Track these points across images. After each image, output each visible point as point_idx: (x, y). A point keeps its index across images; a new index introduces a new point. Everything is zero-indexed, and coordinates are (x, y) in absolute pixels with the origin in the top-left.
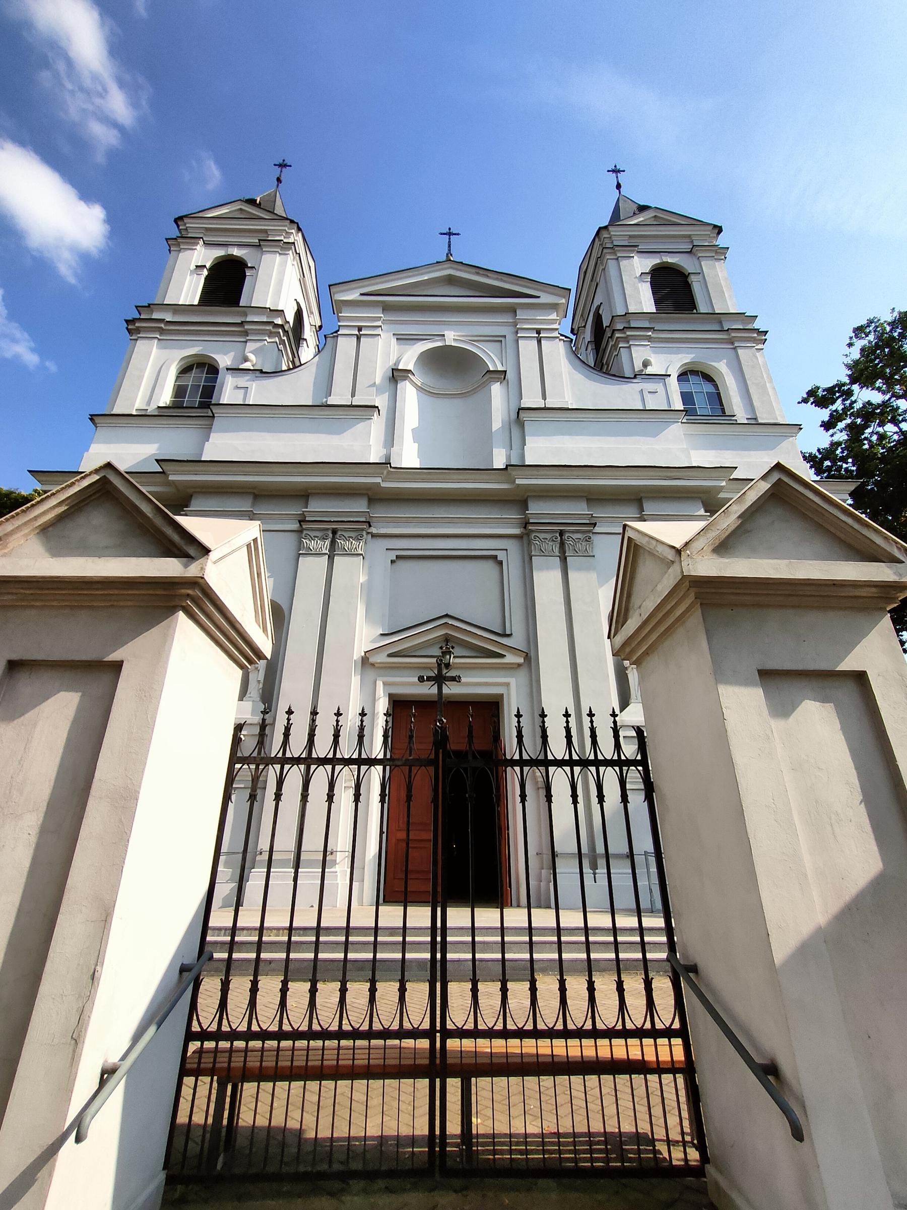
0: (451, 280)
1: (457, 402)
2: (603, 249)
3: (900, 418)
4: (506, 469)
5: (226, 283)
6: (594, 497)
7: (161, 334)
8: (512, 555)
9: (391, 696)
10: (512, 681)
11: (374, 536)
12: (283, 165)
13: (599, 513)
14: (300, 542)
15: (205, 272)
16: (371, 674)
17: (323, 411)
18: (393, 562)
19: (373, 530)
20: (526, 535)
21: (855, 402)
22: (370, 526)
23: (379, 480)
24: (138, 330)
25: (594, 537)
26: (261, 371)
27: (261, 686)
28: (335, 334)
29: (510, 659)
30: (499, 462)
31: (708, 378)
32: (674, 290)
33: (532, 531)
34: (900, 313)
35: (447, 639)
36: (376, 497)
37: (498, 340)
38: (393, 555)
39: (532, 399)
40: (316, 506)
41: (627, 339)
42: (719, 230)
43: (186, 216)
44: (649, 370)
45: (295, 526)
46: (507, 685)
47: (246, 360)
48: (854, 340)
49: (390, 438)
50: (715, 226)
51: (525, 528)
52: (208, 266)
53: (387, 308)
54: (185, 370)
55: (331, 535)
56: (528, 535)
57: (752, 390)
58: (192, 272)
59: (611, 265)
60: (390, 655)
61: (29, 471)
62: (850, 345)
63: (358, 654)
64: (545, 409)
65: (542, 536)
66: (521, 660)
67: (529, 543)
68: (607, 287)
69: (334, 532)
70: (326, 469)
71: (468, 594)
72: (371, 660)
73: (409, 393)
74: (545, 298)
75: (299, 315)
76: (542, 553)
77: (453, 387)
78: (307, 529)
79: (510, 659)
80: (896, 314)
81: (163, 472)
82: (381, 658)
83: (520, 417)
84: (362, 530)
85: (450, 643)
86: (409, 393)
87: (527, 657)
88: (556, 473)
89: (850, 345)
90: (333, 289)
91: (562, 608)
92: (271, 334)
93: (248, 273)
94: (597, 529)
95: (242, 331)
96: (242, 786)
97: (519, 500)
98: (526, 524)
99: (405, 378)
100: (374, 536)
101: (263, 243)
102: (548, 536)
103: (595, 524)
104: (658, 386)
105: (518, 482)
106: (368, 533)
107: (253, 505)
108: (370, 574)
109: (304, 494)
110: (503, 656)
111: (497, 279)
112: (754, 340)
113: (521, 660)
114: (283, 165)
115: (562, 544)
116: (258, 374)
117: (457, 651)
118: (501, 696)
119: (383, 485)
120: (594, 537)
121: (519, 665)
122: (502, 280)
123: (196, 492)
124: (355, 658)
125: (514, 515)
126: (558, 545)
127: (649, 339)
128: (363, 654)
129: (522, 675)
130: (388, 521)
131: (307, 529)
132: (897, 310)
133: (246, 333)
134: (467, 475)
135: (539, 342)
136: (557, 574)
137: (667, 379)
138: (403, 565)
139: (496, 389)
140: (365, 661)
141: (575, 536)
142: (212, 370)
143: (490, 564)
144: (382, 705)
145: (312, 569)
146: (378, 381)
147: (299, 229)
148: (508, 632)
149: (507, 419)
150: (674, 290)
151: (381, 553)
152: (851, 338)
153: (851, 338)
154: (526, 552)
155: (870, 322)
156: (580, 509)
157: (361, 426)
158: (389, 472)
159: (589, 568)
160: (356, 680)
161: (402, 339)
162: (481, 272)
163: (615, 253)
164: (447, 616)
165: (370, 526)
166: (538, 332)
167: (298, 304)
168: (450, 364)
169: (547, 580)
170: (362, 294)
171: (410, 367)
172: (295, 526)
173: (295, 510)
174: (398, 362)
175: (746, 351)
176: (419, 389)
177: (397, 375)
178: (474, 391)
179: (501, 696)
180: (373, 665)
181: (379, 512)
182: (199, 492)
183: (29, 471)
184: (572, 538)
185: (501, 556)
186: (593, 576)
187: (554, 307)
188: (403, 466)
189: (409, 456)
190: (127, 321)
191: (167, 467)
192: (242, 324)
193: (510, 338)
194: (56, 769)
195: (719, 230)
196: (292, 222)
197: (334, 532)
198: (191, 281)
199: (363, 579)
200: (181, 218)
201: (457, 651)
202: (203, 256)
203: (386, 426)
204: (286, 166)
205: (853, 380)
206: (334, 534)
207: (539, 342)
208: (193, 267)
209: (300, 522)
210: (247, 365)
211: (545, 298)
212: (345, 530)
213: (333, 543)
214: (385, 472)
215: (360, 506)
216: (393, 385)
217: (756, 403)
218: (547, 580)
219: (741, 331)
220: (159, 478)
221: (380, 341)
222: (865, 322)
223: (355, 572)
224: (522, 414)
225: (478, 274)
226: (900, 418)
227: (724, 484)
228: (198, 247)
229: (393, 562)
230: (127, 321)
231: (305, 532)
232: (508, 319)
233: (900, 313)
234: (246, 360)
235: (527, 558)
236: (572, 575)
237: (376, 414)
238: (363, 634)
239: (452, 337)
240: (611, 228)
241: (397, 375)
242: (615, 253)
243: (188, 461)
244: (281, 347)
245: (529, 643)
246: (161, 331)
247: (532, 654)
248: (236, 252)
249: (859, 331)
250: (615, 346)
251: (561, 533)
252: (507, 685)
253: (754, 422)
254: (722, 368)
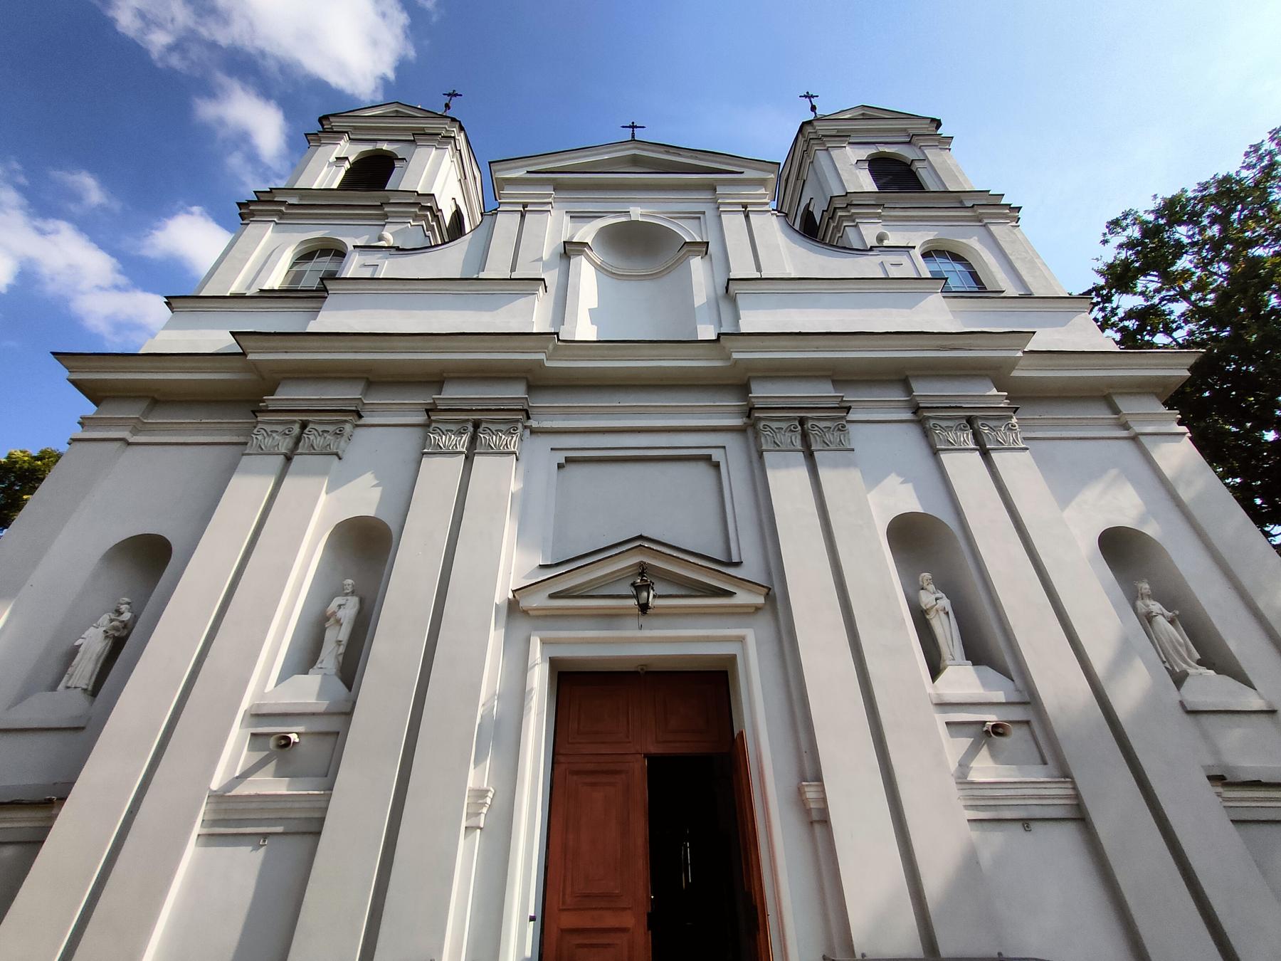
0: (635, 161)
1: (648, 285)
2: (811, 137)
3: (1174, 326)
4: (718, 340)
5: (372, 173)
6: (841, 375)
7: (280, 218)
8: (733, 455)
9: (554, 663)
10: (750, 634)
11: (534, 432)
12: (453, 95)
13: (849, 396)
14: (426, 438)
15: (347, 165)
16: (522, 626)
17: (471, 284)
18: (560, 466)
19: (533, 423)
20: (752, 424)
21: (1118, 307)
22: (529, 418)
23: (542, 356)
24: (252, 214)
25: (848, 426)
26: (398, 249)
27: (342, 649)
28: (495, 212)
29: (743, 598)
30: (707, 332)
31: (957, 258)
32: (896, 176)
33: (760, 419)
34: (1163, 199)
35: (642, 569)
36: (539, 381)
37: (697, 216)
38: (561, 457)
39: (742, 267)
40: (452, 393)
41: (851, 218)
42: (938, 123)
43: (334, 115)
44: (886, 243)
45: (421, 418)
46: (741, 640)
47: (381, 238)
48: (1109, 237)
49: (561, 307)
50: (933, 120)
51: (749, 417)
52: (351, 159)
53: (558, 187)
54: (306, 256)
55: (471, 429)
56: (754, 426)
57: (1018, 265)
58: (330, 164)
59: (821, 157)
60: (552, 596)
61: (53, 353)
62: (1105, 242)
63: (502, 594)
64: (761, 279)
65: (774, 425)
66: (760, 600)
67: (757, 435)
68: (818, 180)
69: (476, 425)
70: (473, 342)
71: (671, 508)
72: (524, 604)
73: (586, 274)
74: (749, 174)
75: (458, 215)
76: (777, 447)
77: (640, 268)
78: (435, 421)
79: (743, 598)
80: (1159, 201)
81: (244, 354)
82: (538, 601)
83: (730, 290)
84: (517, 421)
85: (649, 574)
86: (586, 274)
87: (769, 594)
88: (784, 343)
89: (1105, 242)
90: (494, 167)
91: (816, 521)
92: (416, 217)
93: (397, 164)
94: (851, 416)
95: (381, 214)
96: (280, 829)
97: (737, 384)
98: (749, 412)
99: (581, 253)
100: (534, 432)
101: (419, 137)
102: (784, 425)
103: (849, 409)
104: (903, 259)
105: (735, 356)
106: (525, 427)
107: (365, 393)
108: (527, 478)
109: (436, 378)
110: (729, 594)
111: (691, 157)
112: (1005, 216)
113: (760, 600)
114: (453, 95)
115: (805, 437)
116: (393, 252)
117: (660, 588)
118: (733, 659)
119: (548, 364)
120: (848, 426)
121: (757, 609)
122: (696, 158)
123: (285, 378)
124: (497, 600)
125: (732, 402)
126: (799, 437)
127: (879, 216)
128: (511, 595)
129: (764, 621)
130: (553, 412)
131: (435, 421)
132: (1160, 196)
133: (386, 216)
134: (666, 349)
135: (747, 217)
136: (803, 473)
137: (912, 251)
138: (575, 471)
139: (697, 264)
140: (513, 608)
141: (822, 424)
142: (339, 253)
143: (702, 468)
144: (539, 678)
145: (440, 474)
146: (545, 256)
147: (462, 129)
148: (735, 559)
149: (712, 294)
150: (896, 176)
151: (543, 453)
152: (1104, 234)
153: (1104, 234)
154: (752, 445)
155: (1125, 216)
156: (823, 391)
157: (521, 302)
158: (556, 348)
159: (849, 464)
160: (495, 636)
161: (575, 216)
162: (672, 150)
163: (823, 144)
164: (641, 537)
165: (529, 418)
166: (745, 206)
167: (457, 206)
168: (637, 246)
169: (788, 482)
170: (552, 596)
171: (589, 240)
172: (421, 418)
173: (425, 399)
174: (572, 237)
175: (1000, 227)
176: (599, 268)
177: (570, 250)
178: (668, 270)
179: (733, 659)
180: (525, 612)
181: (539, 402)
182: (289, 378)
183: (53, 353)
184: (818, 426)
185: (717, 455)
186: (855, 475)
187: (762, 183)
188: (577, 339)
189: (584, 330)
190: (239, 204)
191: (249, 343)
192: (381, 206)
193: (710, 213)
194: (1226, 930)
195: (938, 123)
196: (453, 120)
197: (476, 425)
198: (327, 175)
199: (515, 486)
200: (326, 117)
201: (660, 588)
202: (349, 150)
203: (555, 303)
204: (456, 95)
205: (1109, 285)
206: (476, 429)
207: (747, 217)
208: (332, 159)
209: (427, 411)
210: (382, 243)
211: (749, 174)
212: (493, 422)
213: (474, 440)
214: (551, 346)
215: (516, 392)
216: (564, 261)
217: (1027, 278)
218: (788, 482)
219: (988, 208)
220: (237, 362)
221: (550, 219)
222: (1119, 215)
223: (504, 478)
224: (732, 286)
225: (668, 153)
226: (1174, 326)
227: (1020, 354)
228: (342, 142)
229: (560, 466)
230: (239, 204)
231: (434, 425)
232: (707, 195)
233: (1163, 199)
234: (381, 238)
235: (755, 456)
236: (823, 473)
237: (541, 289)
238: (511, 563)
239: (637, 213)
240: (815, 123)
241: (570, 250)
242: (823, 144)
243: (275, 334)
244: (429, 233)
245: (769, 574)
246: (281, 215)
247: (777, 590)
248: (385, 147)
249: (1114, 225)
250: (837, 228)
251: (802, 421)
252: (741, 640)
253: (1028, 296)
254: (972, 242)
